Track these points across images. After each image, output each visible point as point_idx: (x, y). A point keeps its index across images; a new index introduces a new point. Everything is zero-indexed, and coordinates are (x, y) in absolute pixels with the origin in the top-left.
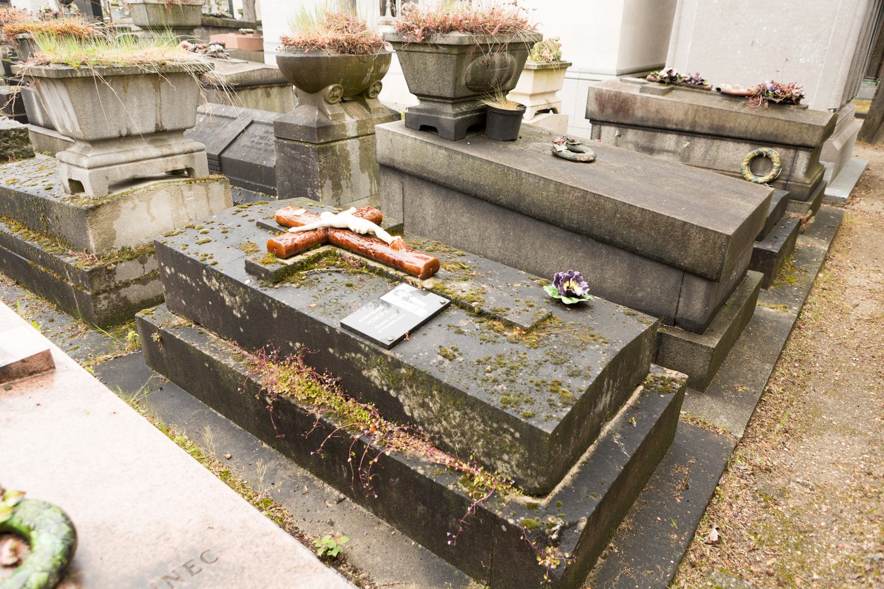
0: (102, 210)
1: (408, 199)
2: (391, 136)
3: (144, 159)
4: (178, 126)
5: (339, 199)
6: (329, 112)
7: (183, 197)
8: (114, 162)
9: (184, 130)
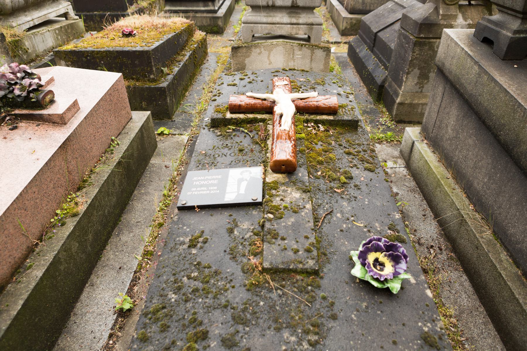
0: (240, 50)
2: (449, 42)
3: (278, 24)
4: (308, 4)
5: (423, 87)
6: (441, 12)
7: (293, 54)
8: (259, 22)
9: (314, 8)
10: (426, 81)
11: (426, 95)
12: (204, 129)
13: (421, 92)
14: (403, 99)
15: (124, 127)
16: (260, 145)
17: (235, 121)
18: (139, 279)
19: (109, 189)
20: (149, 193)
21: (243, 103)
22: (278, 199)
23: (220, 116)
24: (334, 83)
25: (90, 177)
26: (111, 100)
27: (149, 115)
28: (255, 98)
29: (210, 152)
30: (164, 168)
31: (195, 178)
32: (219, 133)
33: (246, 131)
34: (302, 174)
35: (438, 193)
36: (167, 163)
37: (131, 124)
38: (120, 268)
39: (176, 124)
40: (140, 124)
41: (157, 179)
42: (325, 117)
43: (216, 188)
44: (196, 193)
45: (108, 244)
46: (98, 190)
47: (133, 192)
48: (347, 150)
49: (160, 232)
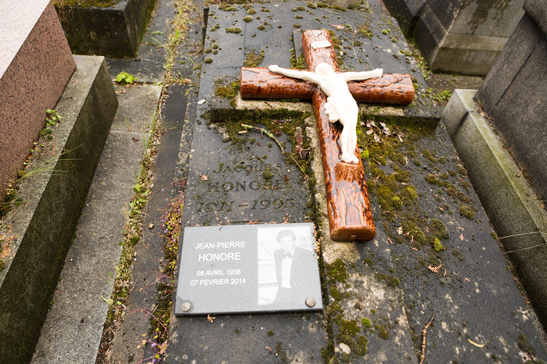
1: (526, 72)
5: (476, 28)
10: (482, 20)
11: (478, 38)
12: (200, 123)
13: (473, 34)
14: (447, 42)
15: (66, 86)
16: (297, 167)
17: (251, 114)
18: (113, 337)
19: (51, 203)
20: (113, 186)
21: (263, 85)
22: (351, 304)
23: (225, 105)
24: (384, 34)
25: (18, 188)
26: (37, 50)
27: (102, 64)
28: (284, 77)
29: (216, 177)
30: (132, 141)
31: (199, 246)
32: (226, 136)
33: (271, 135)
34: (380, 242)
35: (503, 195)
36: (135, 134)
37: (75, 82)
38: (82, 321)
39: (142, 66)
40: (89, 81)
41: (123, 161)
42: (390, 111)
43: (238, 272)
44: (205, 282)
45: (60, 280)
46: (32, 214)
47: (89, 186)
48: (430, 175)
49: (135, 254)
